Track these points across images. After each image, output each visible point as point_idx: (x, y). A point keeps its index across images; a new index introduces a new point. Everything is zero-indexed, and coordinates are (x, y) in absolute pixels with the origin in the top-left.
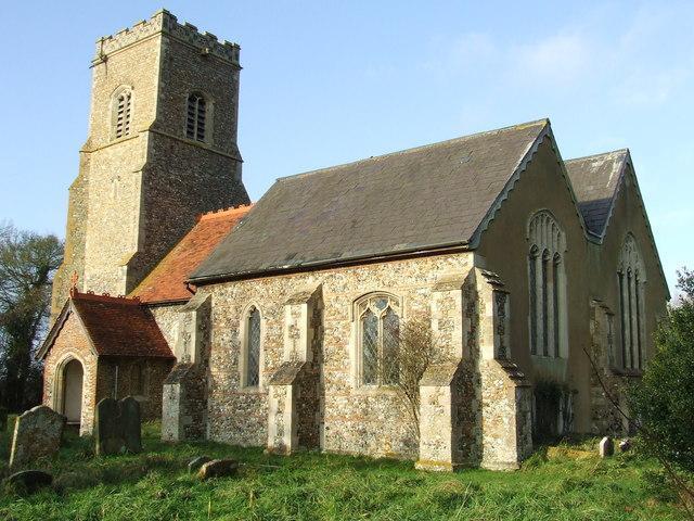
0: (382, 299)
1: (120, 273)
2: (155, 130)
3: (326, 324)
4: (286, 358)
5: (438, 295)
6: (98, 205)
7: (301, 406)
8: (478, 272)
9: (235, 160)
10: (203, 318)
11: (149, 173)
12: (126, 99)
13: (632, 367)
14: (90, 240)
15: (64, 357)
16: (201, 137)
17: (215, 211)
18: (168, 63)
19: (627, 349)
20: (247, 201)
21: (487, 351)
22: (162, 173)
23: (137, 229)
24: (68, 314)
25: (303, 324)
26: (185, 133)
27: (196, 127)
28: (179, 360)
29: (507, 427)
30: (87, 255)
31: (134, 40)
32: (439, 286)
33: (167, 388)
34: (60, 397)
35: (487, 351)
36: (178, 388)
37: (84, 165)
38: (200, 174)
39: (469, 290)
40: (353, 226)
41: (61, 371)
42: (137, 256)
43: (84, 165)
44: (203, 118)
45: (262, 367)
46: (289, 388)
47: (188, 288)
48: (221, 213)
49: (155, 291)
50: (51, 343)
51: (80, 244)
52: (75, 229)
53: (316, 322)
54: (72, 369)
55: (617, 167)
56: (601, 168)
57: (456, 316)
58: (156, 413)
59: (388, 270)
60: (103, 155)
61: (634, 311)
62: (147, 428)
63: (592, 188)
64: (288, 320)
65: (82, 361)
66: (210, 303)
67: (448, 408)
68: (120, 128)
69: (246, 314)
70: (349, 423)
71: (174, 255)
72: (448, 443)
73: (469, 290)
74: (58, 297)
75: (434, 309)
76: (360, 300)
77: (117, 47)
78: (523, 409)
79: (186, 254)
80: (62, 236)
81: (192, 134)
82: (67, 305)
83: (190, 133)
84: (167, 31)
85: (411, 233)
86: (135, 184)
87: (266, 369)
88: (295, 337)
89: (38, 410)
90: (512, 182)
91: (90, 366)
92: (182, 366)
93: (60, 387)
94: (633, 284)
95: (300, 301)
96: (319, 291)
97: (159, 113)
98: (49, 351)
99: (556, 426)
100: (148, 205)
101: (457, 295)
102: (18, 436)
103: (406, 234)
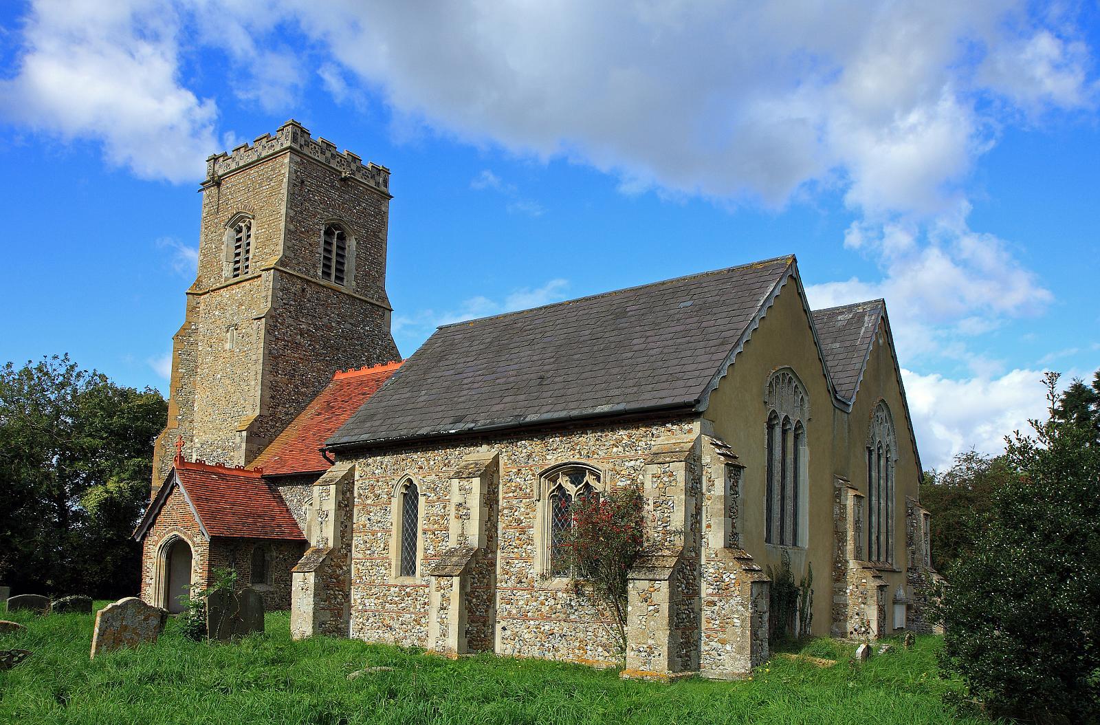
0: (577, 473)
1: (238, 440)
2: (281, 270)
3: (502, 503)
4: (452, 543)
5: (655, 469)
6: (210, 359)
7: (470, 602)
8: (706, 439)
9: (382, 309)
10: (344, 493)
11: (273, 321)
12: (244, 229)
13: (878, 559)
14: (200, 399)
15: (166, 537)
16: (339, 279)
17: (359, 368)
18: (298, 185)
19: (874, 537)
20: (396, 357)
21: (714, 539)
22: (290, 321)
23: (259, 388)
24: (173, 488)
25: (475, 502)
26: (320, 274)
27: (334, 266)
28: (313, 543)
29: (739, 631)
30: (197, 417)
31: (255, 158)
32: (655, 458)
33: (297, 578)
34: (162, 585)
35: (714, 539)
36: (311, 577)
37: (193, 310)
38: (339, 323)
39: (693, 461)
40: (540, 384)
41: (164, 555)
42: (260, 419)
43: (193, 310)
44: (342, 264)
45: (420, 555)
46: (456, 581)
47: (325, 456)
48: (365, 371)
49: (282, 462)
50: (151, 521)
51: (188, 404)
52: (178, 384)
53: (490, 500)
54: (177, 552)
55: (869, 321)
56: (849, 322)
57: (679, 496)
58: (284, 603)
59: (587, 441)
60: (216, 298)
61: (883, 495)
62: (272, 620)
63: (838, 345)
64: (456, 498)
65: (189, 542)
66: (353, 476)
67: (665, 608)
68: (237, 266)
69: (602, 480)
70: (532, 622)
71: (305, 418)
72: (664, 650)
73: (693, 461)
74: (161, 464)
75: (648, 485)
76: (551, 474)
77: (233, 166)
78: (759, 609)
79: (321, 418)
80: (166, 395)
81: (329, 275)
82: (171, 475)
83: (326, 274)
84: (297, 147)
85: (617, 392)
86: (256, 334)
87: (426, 558)
88: (463, 517)
89: (126, 603)
90: (750, 331)
91: (200, 550)
92: (318, 551)
93: (163, 573)
94: (882, 462)
95: (470, 476)
96: (496, 461)
97: (287, 248)
98: (149, 529)
99: (793, 628)
100: (273, 359)
101: (679, 470)
102: (99, 634)
103: (612, 393)
